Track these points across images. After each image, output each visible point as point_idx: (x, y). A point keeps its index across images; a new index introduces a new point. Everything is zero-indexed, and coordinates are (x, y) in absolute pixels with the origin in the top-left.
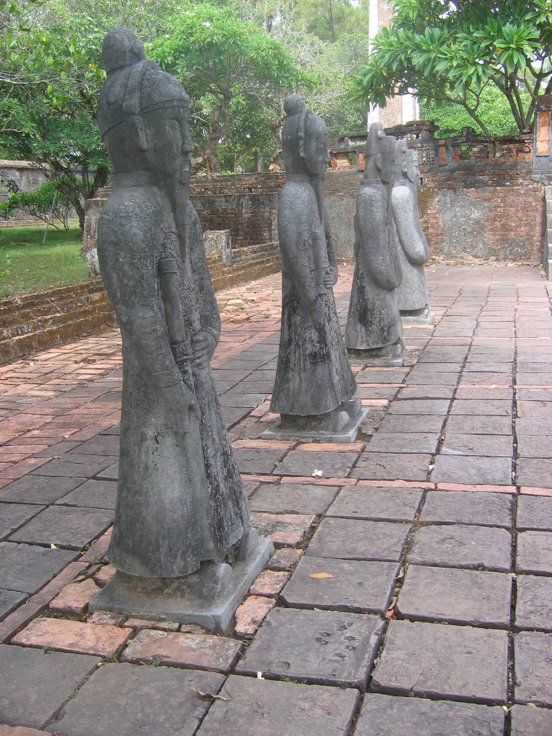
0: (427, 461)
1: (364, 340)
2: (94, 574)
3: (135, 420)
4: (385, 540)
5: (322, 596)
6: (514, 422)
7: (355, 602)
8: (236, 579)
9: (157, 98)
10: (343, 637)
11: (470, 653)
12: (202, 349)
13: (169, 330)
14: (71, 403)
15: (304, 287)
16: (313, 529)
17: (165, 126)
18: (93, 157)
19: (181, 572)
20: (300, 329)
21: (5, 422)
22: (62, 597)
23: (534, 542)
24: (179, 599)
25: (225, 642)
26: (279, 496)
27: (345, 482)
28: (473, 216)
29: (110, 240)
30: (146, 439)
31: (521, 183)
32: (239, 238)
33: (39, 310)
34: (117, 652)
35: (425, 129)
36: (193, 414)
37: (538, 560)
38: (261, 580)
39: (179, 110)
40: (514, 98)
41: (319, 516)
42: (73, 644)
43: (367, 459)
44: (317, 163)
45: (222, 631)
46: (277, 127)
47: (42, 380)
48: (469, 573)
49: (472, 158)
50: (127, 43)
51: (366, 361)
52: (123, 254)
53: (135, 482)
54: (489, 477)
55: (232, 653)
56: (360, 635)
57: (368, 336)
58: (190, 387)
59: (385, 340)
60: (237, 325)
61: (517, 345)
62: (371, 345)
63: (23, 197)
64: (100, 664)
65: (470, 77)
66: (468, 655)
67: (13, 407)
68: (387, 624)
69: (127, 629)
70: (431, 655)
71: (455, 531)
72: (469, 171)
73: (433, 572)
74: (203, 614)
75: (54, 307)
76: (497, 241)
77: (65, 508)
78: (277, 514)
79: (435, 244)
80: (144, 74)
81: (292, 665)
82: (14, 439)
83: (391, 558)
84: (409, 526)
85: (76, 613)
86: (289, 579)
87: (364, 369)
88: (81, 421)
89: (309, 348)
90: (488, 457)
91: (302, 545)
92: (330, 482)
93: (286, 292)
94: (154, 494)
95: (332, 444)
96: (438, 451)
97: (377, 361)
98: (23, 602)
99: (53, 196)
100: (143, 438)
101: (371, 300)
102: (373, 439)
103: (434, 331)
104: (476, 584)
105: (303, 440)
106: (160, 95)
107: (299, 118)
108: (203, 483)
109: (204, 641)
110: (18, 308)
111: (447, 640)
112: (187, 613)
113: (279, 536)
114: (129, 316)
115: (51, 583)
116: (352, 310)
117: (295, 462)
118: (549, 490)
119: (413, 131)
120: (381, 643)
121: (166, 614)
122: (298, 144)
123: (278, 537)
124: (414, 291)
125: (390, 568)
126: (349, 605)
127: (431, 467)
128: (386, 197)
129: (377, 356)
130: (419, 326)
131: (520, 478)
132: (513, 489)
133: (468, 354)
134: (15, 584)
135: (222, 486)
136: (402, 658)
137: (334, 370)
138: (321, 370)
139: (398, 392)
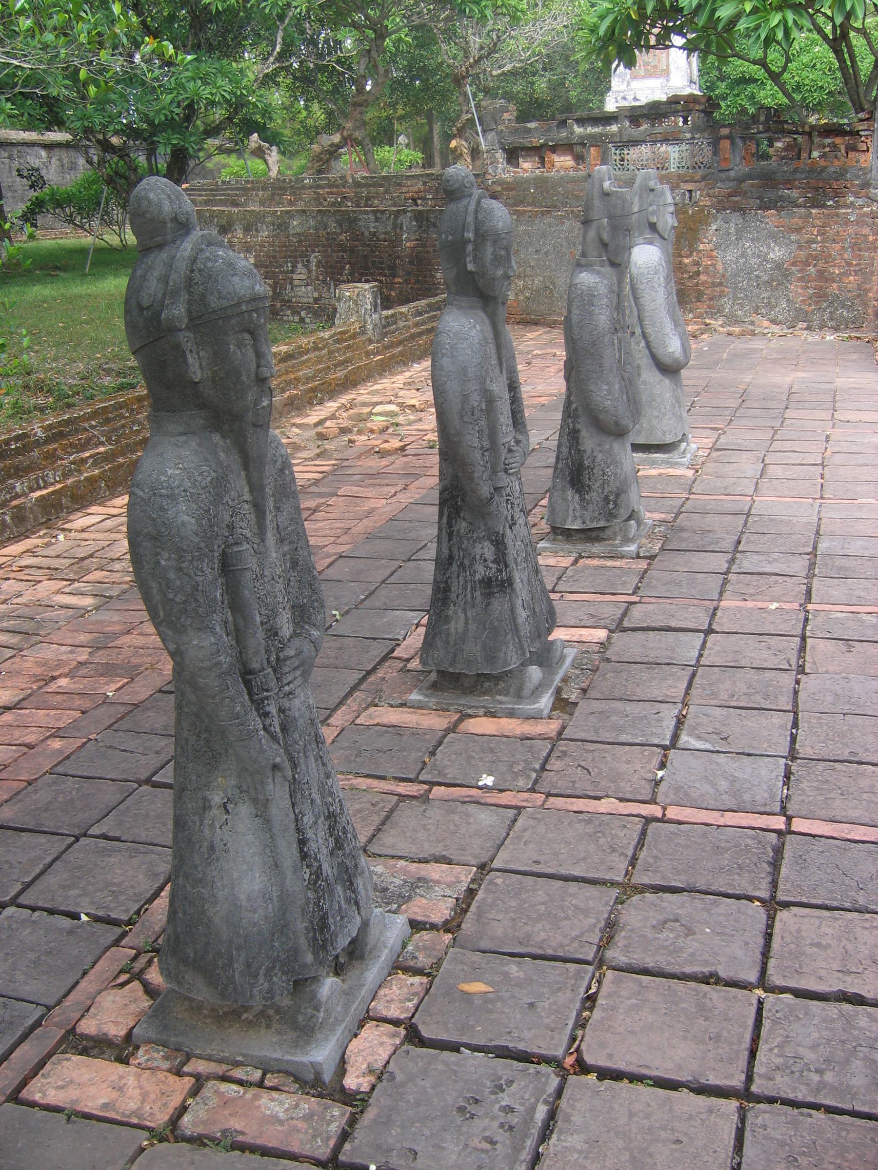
0: (656, 761)
1: (578, 514)
2: (142, 971)
3: (194, 778)
4: (576, 921)
5: (473, 1027)
6: (798, 682)
7: (521, 1039)
8: (349, 994)
9: (214, 303)
10: (497, 1106)
11: (678, 1141)
12: (294, 669)
13: (240, 653)
14: (118, 623)
15: (472, 479)
16: (471, 893)
17: (229, 344)
18: (164, 131)
19: (265, 999)
20: (466, 542)
21: (17, 659)
22: (95, 1015)
23: (799, 931)
24: (263, 1031)
25: (326, 1108)
26: (424, 827)
27: (527, 800)
28: (772, 255)
29: (146, 531)
30: (210, 807)
31: (852, 203)
32: (396, 280)
33: (71, 444)
34: (171, 1119)
35: (700, 110)
36: (280, 774)
37: (801, 967)
38: (387, 991)
39: (250, 316)
40: (846, 56)
41: (482, 867)
42: (108, 1104)
43: (564, 753)
44: (494, 279)
45: (324, 1083)
46: (464, 78)
47: (76, 573)
48: (694, 990)
49: (774, 158)
50: (167, 207)
51: (580, 547)
52: (166, 555)
53: (196, 867)
54: (747, 797)
55: (334, 1128)
56: (522, 1104)
57: (584, 508)
58: (274, 738)
59: (611, 516)
60: (384, 462)
61: (822, 515)
62: (588, 523)
63: (53, 194)
64: (146, 1143)
65: (773, 30)
66: (674, 1146)
67: (29, 629)
68: (564, 1079)
69: (187, 1079)
70: (621, 1144)
71: (682, 906)
72: (769, 180)
73: (640, 984)
74: (297, 1059)
75: (95, 436)
76: (810, 298)
77: (103, 843)
78: (420, 862)
79: (711, 299)
80: (194, 261)
81: (420, 1154)
82: (30, 695)
83: (581, 956)
84: (615, 892)
85: (114, 1044)
86: (428, 991)
87: (576, 562)
88: (135, 661)
89: (481, 571)
90: (749, 755)
91: (450, 926)
92: (505, 798)
93: (445, 483)
94: (223, 886)
95: (513, 720)
96: (673, 745)
97: (597, 548)
98: (37, 1024)
99: (102, 192)
100: (206, 806)
101: (589, 452)
102: (578, 711)
103: (695, 481)
104: (704, 1011)
105: (470, 711)
106: (220, 298)
107: (466, 207)
108: (295, 872)
109: (297, 1106)
110: (38, 443)
111: (647, 1116)
112: (274, 1056)
113: (418, 908)
114: (177, 644)
115: (79, 987)
116: (560, 466)
117: (453, 757)
118: (835, 825)
119: (678, 111)
120: (552, 1115)
121: (244, 1055)
122: (464, 249)
123: (417, 910)
124: (664, 414)
125: (578, 976)
126: (511, 1045)
127: (660, 774)
128: (615, 288)
129: (598, 539)
130: (672, 471)
131: (795, 799)
132: (779, 823)
133: (742, 533)
134: (27, 988)
135: (325, 866)
136: (579, 1147)
137: (520, 602)
138: (499, 605)
139: (625, 614)
